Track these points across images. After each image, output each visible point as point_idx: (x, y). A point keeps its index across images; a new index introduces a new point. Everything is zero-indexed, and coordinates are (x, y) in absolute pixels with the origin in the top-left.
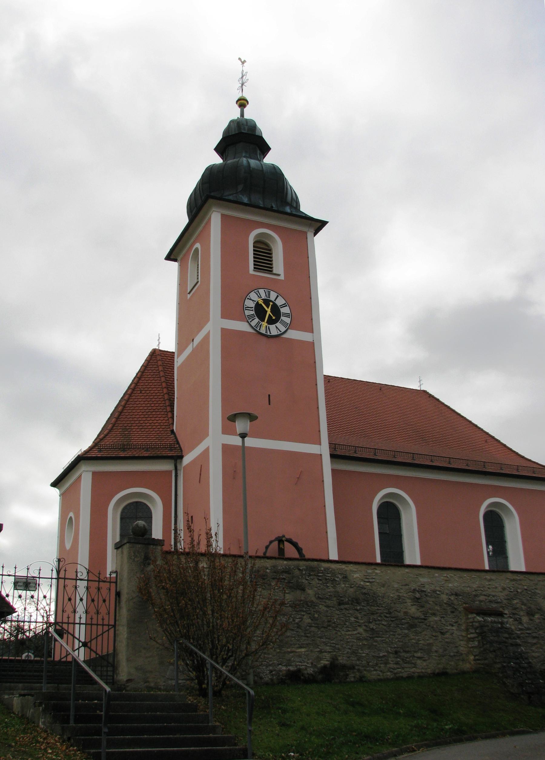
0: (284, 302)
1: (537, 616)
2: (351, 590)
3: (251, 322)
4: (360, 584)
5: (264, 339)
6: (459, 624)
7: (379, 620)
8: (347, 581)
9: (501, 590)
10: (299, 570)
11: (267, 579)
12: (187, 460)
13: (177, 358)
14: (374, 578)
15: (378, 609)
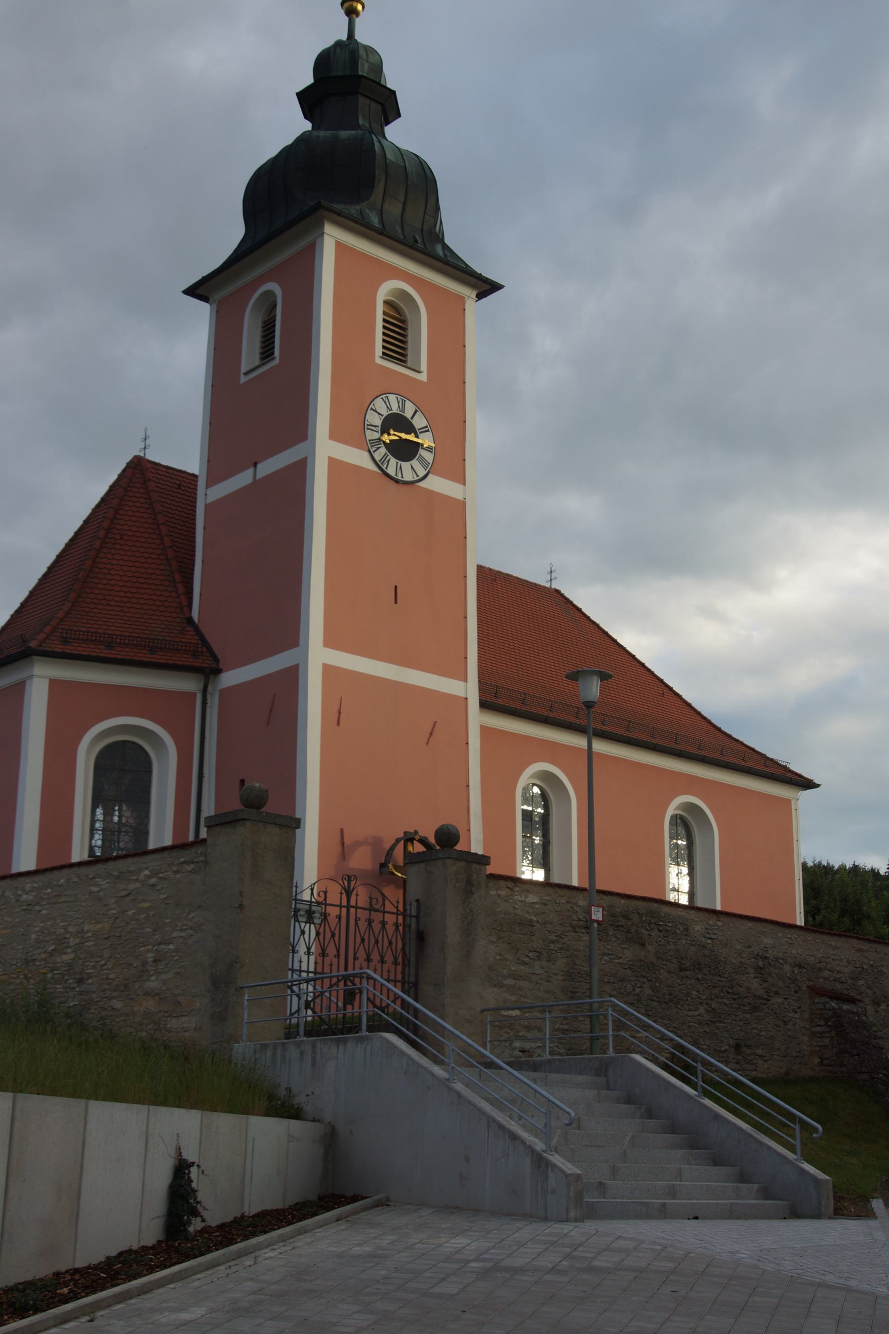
0: (424, 423)
1: (883, 1007)
2: (692, 948)
3: (374, 451)
4: (701, 942)
6: (802, 1011)
7: (721, 997)
9: (846, 964)
10: (639, 913)
12: (230, 678)
14: (716, 934)
15: (719, 981)
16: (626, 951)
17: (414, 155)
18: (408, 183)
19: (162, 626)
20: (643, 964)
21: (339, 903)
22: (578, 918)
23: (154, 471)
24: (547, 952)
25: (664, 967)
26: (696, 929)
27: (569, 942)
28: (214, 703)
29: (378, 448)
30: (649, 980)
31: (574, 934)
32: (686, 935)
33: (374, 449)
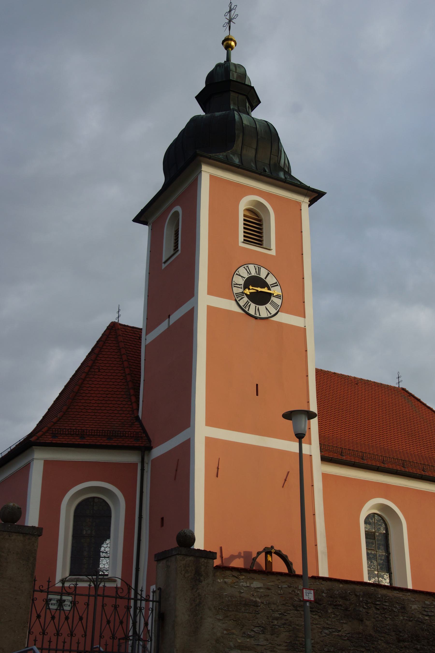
0: (275, 281)
2: (410, 623)
3: (239, 300)
4: (419, 618)
5: (253, 319)
8: (406, 613)
11: (323, 605)
13: (146, 335)
16: (345, 626)
17: (264, 121)
18: (259, 137)
19: (120, 423)
20: (360, 636)
21: (87, 593)
22: (299, 599)
23: (123, 330)
24: (271, 627)
25: (382, 638)
26: (413, 608)
27: (291, 619)
28: (148, 468)
29: (242, 298)
30: (367, 650)
31: (296, 612)
32: (403, 612)
33: (239, 299)
